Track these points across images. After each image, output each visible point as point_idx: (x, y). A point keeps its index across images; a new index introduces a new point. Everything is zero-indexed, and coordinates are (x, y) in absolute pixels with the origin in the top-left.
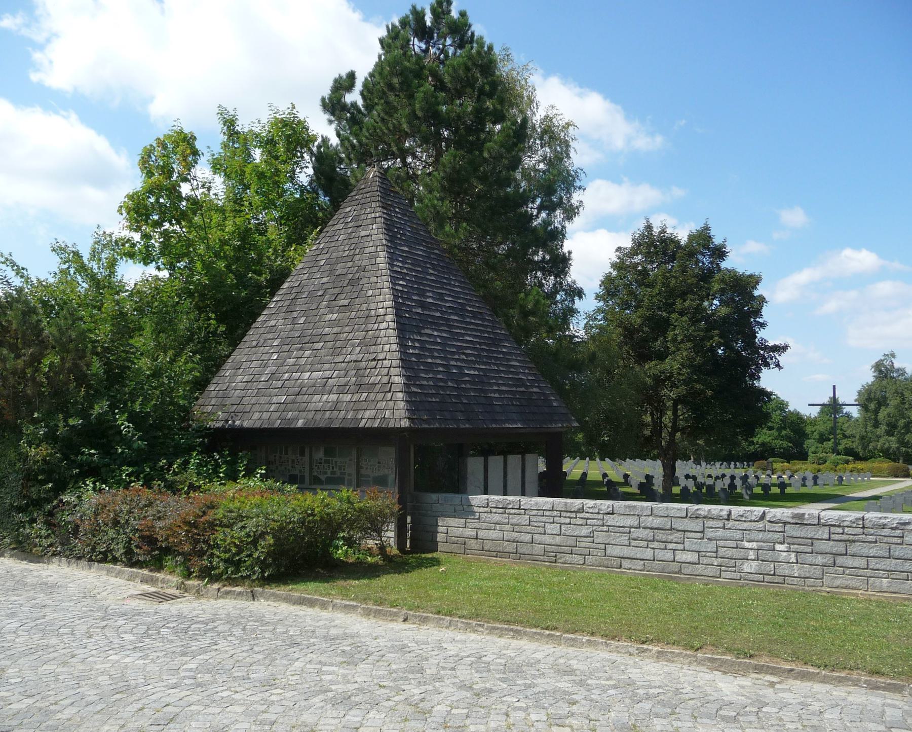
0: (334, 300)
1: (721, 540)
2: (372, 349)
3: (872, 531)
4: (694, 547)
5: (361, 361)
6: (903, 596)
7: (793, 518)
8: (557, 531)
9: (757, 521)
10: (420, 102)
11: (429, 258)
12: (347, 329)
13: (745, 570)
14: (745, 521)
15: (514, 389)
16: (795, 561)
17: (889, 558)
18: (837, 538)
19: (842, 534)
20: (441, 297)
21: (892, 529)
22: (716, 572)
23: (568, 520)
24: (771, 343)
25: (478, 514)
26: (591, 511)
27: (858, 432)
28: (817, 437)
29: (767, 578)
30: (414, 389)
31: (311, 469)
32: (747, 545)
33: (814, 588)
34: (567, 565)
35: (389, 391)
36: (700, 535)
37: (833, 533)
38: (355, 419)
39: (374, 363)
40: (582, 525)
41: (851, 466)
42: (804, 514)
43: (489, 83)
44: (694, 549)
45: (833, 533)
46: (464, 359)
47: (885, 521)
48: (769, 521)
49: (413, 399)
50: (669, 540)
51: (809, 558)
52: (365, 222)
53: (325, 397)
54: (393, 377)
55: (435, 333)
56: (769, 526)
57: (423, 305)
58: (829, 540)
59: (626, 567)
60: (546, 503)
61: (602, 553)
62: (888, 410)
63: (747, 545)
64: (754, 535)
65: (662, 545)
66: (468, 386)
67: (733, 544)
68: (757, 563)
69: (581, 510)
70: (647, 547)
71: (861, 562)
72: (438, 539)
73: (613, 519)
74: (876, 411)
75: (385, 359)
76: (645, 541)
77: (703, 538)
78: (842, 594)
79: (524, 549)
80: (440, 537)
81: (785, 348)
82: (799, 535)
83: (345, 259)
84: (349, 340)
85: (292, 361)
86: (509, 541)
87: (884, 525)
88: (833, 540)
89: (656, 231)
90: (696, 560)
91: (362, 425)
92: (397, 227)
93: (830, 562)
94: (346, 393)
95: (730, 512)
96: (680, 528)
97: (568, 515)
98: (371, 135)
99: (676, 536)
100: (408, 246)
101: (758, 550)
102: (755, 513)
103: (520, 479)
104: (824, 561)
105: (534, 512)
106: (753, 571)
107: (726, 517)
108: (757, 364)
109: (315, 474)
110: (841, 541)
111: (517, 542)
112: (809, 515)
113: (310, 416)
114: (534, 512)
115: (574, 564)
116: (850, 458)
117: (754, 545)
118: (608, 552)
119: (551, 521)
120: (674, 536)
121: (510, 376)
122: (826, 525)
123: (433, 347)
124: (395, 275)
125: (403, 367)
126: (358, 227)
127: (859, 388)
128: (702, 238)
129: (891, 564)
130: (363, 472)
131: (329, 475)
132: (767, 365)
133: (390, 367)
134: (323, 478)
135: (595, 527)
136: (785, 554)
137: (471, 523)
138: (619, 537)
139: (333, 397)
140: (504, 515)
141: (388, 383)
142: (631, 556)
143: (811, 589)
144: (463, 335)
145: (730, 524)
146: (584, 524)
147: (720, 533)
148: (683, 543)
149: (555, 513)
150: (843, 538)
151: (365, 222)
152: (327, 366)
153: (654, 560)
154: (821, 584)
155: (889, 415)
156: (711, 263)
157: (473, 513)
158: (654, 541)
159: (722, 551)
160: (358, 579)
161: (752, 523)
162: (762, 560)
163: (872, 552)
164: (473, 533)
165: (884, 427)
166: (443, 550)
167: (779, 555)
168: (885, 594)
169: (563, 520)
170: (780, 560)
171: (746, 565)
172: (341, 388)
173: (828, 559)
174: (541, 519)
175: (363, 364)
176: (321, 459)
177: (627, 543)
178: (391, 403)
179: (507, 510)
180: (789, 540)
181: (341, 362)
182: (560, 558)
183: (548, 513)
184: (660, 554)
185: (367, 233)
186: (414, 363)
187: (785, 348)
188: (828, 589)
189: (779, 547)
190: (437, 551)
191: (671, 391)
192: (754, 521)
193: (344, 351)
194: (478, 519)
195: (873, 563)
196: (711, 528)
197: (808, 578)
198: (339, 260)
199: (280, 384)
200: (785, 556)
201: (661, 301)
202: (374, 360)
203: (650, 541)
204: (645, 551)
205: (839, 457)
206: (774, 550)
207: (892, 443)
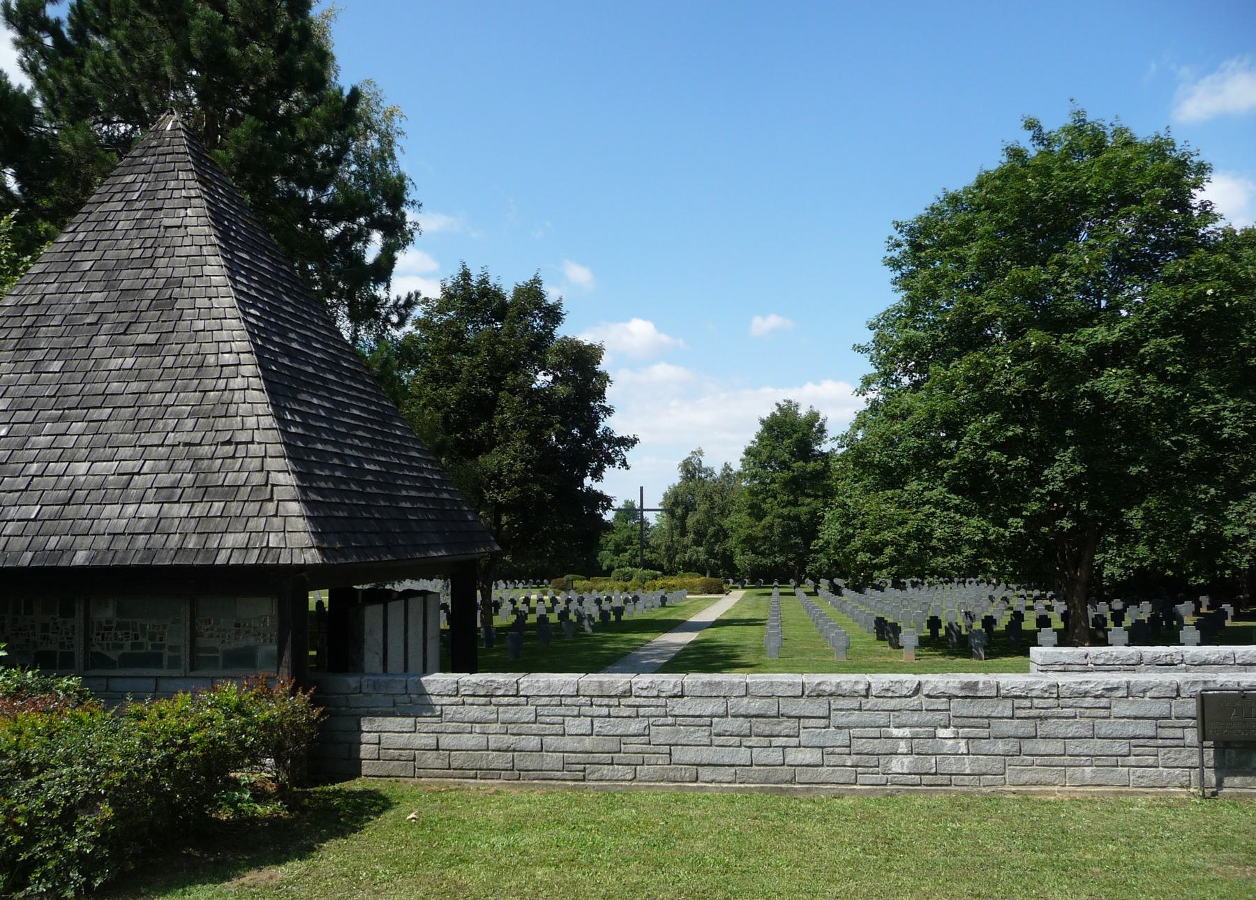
0: (124, 333)
1: (857, 727)
2: (221, 423)
3: (1071, 702)
4: (815, 742)
5: (200, 444)
6: (1112, 789)
7: (962, 689)
8: (586, 728)
9: (910, 697)
10: (198, 35)
11: (277, 276)
12: (159, 386)
13: (894, 770)
14: (891, 697)
15: (423, 495)
16: (965, 752)
17: (1093, 738)
18: (1023, 715)
19: (1030, 708)
20: (306, 342)
21: (1096, 697)
22: (850, 776)
23: (605, 711)
24: (617, 435)
25: (438, 708)
26: (645, 693)
27: (663, 541)
28: (613, 548)
29: (926, 779)
30: (313, 496)
31: (88, 641)
32: (896, 732)
33: (993, 789)
34: (604, 783)
35: (271, 500)
36: (823, 722)
37: (1018, 708)
38: (204, 549)
39: (229, 449)
40: (629, 717)
41: (660, 583)
42: (976, 683)
43: (298, 29)
44: (816, 744)
45: (1018, 708)
46: (358, 446)
47: (1088, 687)
48: (928, 696)
49: (316, 514)
50: (775, 733)
51: (986, 746)
52: (168, 204)
53: (130, 509)
54: (272, 474)
55: (315, 401)
56: (926, 703)
57: (288, 352)
58: (1012, 718)
59: (706, 778)
60: (566, 683)
61: (663, 759)
62: (698, 517)
63: (896, 732)
64: (905, 718)
65: (765, 742)
66: (374, 490)
67: (874, 732)
68: (910, 758)
69: (628, 693)
70: (740, 746)
71: (1056, 746)
72: (362, 755)
73: (684, 704)
74: (683, 518)
75: (252, 442)
76: (737, 736)
77: (828, 727)
78: (1034, 793)
79: (529, 762)
80: (366, 751)
81: (633, 442)
82: (970, 714)
83: (136, 264)
84: (167, 406)
85: (43, 441)
86: (499, 750)
87: (1086, 693)
88: (1018, 718)
89: (475, 280)
90: (819, 761)
91: (221, 559)
92: (227, 220)
93: (1015, 749)
94: (178, 502)
95: (869, 685)
96: (793, 713)
97: (606, 701)
98: (99, 75)
99: (787, 726)
100: (247, 253)
101: (912, 738)
102: (906, 685)
103: (421, 635)
104: (1007, 748)
105: (545, 700)
106: (905, 771)
107: (864, 693)
108: (600, 460)
109: (97, 649)
110: (1029, 718)
111: (514, 750)
112: (984, 683)
113: (102, 543)
114: (545, 700)
115: (617, 780)
116: (658, 573)
117: (906, 732)
118: (675, 758)
119: (576, 713)
120: (783, 726)
121: (415, 474)
122: (1007, 697)
123: (318, 424)
124: (241, 298)
125: (289, 458)
126: (155, 210)
127: (665, 489)
128: (531, 294)
129: (1096, 746)
130: (203, 642)
131: (127, 649)
132: (612, 462)
133: (265, 457)
134: (114, 655)
135: (651, 720)
136: (951, 742)
137: (426, 723)
138: (694, 732)
139: (150, 510)
140: (488, 708)
141: (266, 485)
142: (714, 761)
143: (989, 790)
144: (349, 406)
145: (872, 701)
146: (634, 714)
147: (855, 717)
148: (798, 737)
149: (582, 700)
150: (1031, 715)
151: (168, 204)
152: (125, 452)
153: (751, 765)
154: (1002, 782)
155: (698, 521)
156: (543, 327)
157: (430, 707)
158: (750, 736)
159: (858, 745)
160: (279, 862)
161: (903, 699)
162: (918, 754)
163: (1071, 732)
164: (430, 741)
165: (691, 536)
166: (373, 773)
167: (943, 744)
168: (1088, 789)
169: (596, 711)
170: (944, 751)
171: (894, 761)
172: (164, 492)
173: (1011, 746)
174: (557, 710)
175: (206, 450)
176: (108, 622)
177: (707, 741)
178: (277, 522)
179: (494, 700)
180: (957, 721)
181: (158, 446)
182: (593, 772)
183: (569, 701)
184: (761, 756)
185: (177, 222)
186: (301, 450)
187: (633, 442)
188: (1013, 789)
189: (942, 733)
190: (359, 775)
191: (498, 494)
192: (906, 697)
193: (160, 424)
194: (440, 716)
195: (1073, 747)
196: (841, 710)
197: (984, 774)
198: (120, 264)
199: (21, 483)
200: (952, 745)
201: (484, 374)
202: (229, 442)
203: (745, 736)
204: (738, 752)
205: (646, 572)
206: (935, 737)
207: (700, 553)
